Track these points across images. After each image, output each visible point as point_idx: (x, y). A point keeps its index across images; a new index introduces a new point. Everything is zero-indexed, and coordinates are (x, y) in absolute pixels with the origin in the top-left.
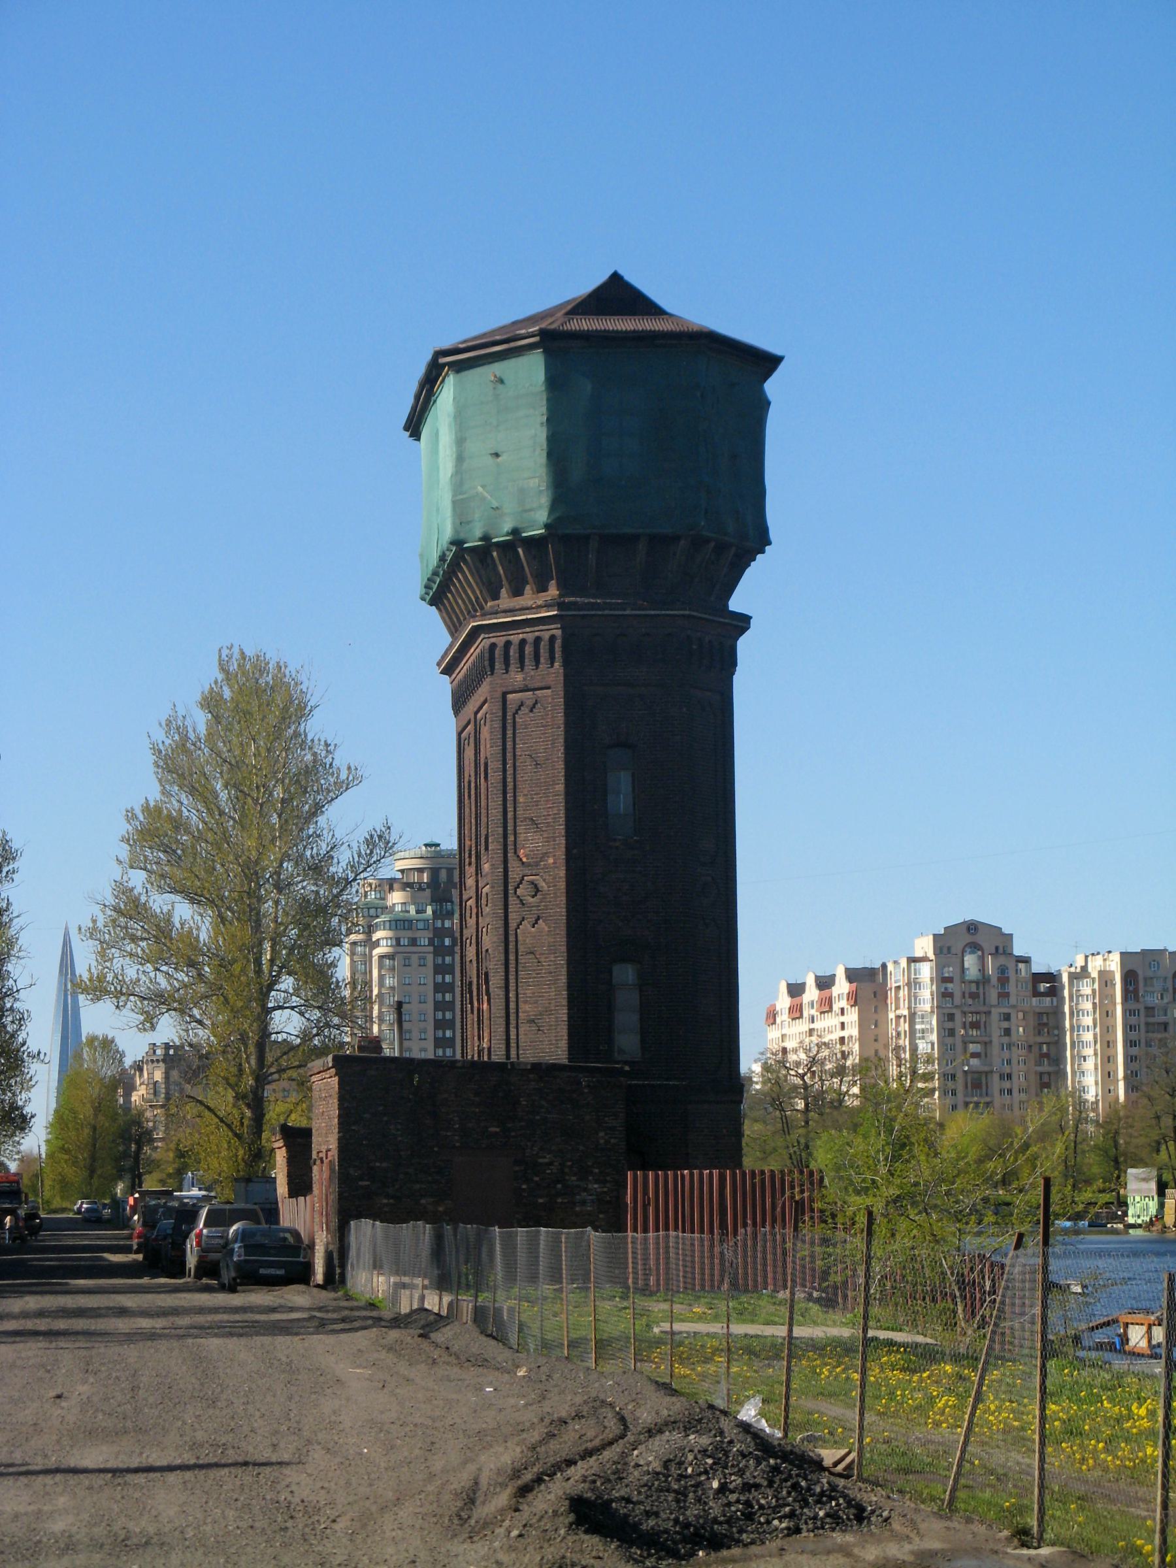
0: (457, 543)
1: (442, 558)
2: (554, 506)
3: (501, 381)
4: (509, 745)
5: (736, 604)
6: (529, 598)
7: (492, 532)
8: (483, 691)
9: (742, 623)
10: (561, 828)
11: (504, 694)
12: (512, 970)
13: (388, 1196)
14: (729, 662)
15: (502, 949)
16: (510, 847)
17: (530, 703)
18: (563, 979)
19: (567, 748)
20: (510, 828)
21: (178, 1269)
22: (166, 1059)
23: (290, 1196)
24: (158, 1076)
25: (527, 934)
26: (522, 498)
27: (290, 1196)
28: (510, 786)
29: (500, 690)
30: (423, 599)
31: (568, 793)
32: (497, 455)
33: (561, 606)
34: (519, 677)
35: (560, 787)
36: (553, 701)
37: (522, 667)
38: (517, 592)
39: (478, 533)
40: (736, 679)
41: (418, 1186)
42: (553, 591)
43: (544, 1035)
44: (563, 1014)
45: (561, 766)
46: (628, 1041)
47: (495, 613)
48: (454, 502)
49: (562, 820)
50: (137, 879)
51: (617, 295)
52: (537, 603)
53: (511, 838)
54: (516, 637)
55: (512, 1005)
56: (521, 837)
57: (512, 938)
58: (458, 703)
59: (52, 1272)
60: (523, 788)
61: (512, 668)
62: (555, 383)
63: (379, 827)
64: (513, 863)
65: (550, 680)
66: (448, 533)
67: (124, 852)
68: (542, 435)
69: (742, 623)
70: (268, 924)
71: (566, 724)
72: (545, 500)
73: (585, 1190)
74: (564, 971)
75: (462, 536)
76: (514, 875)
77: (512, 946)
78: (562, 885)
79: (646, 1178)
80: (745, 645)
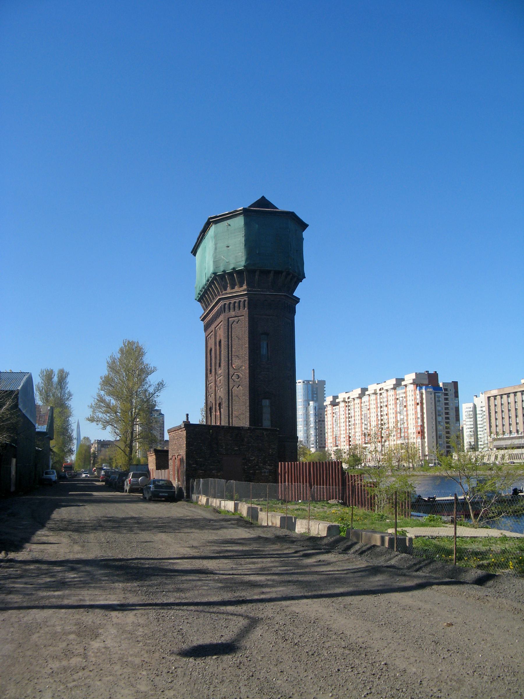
0: (215, 273)
1: (208, 281)
2: (247, 260)
3: (230, 225)
4: (230, 333)
5: (295, 294)
6: (237, 288)
7: (226, 270)
8: (221, 318)
9: (297, 300)
10: (247, 358)
11: (228, 318)
12: (230, 401)
13: (202, 470)
14: (293, 312)
15: (227, 395)
16: (230, 364)
17: (237, 321)
18: (248, 404)
19: (249, 333)
20: (230, 358)
21: (121, 489)
22: (98, 442)
23: (157, 469)
24: (96, 446)
25: (235, 390)
26: (236, 257)
27: (157, 469)
28: (230, 346)
29: (227, 318)
30: (196, 300)
31: (249, 347)
32: (228, 247)
33: (248, 291)
34: (233, 313)
35: (247, 345)
36: (245, 320)
37: (234, 310)
38: (233, 288)
39: (222, 270)
40: (296, 317)
41: (212, 467)
42: (245, 287)
43: (242, 419)
44: (248, 414)
45: (247, 339)
46: (267, 423)
47: (227, 294)
48: (214, 262)
49: (248, 355)
50: (102, 393)
51: (263, 202)
52: (241, 290)
53: (230, 362)
54: (232, 301)
55: (230, 412)
56: (233, 361)
57: (230, 392)
58: (206, 328)
59: (110, 521)
60: (234, 347)
61: (231, 310)
62: (247, 224)
63: (161, 381)
64: (231, 369)
65: (244, 313)
66: (211, 270)
67: (99, 387)
68: (243, 240)
69: (297, 300)
70: (134, 404)
71: (249, 326)
72: (244, 259)
73: (266, 468)
74: (248, 401)
75: (216, 271)
76: (231, 373)
77: (230, 394)
78: (247, 375)
79: (285, 465)
80: (298, 306)
